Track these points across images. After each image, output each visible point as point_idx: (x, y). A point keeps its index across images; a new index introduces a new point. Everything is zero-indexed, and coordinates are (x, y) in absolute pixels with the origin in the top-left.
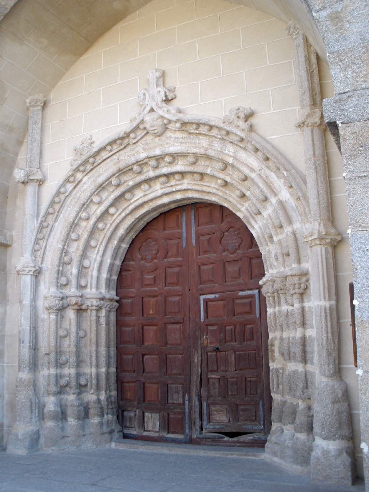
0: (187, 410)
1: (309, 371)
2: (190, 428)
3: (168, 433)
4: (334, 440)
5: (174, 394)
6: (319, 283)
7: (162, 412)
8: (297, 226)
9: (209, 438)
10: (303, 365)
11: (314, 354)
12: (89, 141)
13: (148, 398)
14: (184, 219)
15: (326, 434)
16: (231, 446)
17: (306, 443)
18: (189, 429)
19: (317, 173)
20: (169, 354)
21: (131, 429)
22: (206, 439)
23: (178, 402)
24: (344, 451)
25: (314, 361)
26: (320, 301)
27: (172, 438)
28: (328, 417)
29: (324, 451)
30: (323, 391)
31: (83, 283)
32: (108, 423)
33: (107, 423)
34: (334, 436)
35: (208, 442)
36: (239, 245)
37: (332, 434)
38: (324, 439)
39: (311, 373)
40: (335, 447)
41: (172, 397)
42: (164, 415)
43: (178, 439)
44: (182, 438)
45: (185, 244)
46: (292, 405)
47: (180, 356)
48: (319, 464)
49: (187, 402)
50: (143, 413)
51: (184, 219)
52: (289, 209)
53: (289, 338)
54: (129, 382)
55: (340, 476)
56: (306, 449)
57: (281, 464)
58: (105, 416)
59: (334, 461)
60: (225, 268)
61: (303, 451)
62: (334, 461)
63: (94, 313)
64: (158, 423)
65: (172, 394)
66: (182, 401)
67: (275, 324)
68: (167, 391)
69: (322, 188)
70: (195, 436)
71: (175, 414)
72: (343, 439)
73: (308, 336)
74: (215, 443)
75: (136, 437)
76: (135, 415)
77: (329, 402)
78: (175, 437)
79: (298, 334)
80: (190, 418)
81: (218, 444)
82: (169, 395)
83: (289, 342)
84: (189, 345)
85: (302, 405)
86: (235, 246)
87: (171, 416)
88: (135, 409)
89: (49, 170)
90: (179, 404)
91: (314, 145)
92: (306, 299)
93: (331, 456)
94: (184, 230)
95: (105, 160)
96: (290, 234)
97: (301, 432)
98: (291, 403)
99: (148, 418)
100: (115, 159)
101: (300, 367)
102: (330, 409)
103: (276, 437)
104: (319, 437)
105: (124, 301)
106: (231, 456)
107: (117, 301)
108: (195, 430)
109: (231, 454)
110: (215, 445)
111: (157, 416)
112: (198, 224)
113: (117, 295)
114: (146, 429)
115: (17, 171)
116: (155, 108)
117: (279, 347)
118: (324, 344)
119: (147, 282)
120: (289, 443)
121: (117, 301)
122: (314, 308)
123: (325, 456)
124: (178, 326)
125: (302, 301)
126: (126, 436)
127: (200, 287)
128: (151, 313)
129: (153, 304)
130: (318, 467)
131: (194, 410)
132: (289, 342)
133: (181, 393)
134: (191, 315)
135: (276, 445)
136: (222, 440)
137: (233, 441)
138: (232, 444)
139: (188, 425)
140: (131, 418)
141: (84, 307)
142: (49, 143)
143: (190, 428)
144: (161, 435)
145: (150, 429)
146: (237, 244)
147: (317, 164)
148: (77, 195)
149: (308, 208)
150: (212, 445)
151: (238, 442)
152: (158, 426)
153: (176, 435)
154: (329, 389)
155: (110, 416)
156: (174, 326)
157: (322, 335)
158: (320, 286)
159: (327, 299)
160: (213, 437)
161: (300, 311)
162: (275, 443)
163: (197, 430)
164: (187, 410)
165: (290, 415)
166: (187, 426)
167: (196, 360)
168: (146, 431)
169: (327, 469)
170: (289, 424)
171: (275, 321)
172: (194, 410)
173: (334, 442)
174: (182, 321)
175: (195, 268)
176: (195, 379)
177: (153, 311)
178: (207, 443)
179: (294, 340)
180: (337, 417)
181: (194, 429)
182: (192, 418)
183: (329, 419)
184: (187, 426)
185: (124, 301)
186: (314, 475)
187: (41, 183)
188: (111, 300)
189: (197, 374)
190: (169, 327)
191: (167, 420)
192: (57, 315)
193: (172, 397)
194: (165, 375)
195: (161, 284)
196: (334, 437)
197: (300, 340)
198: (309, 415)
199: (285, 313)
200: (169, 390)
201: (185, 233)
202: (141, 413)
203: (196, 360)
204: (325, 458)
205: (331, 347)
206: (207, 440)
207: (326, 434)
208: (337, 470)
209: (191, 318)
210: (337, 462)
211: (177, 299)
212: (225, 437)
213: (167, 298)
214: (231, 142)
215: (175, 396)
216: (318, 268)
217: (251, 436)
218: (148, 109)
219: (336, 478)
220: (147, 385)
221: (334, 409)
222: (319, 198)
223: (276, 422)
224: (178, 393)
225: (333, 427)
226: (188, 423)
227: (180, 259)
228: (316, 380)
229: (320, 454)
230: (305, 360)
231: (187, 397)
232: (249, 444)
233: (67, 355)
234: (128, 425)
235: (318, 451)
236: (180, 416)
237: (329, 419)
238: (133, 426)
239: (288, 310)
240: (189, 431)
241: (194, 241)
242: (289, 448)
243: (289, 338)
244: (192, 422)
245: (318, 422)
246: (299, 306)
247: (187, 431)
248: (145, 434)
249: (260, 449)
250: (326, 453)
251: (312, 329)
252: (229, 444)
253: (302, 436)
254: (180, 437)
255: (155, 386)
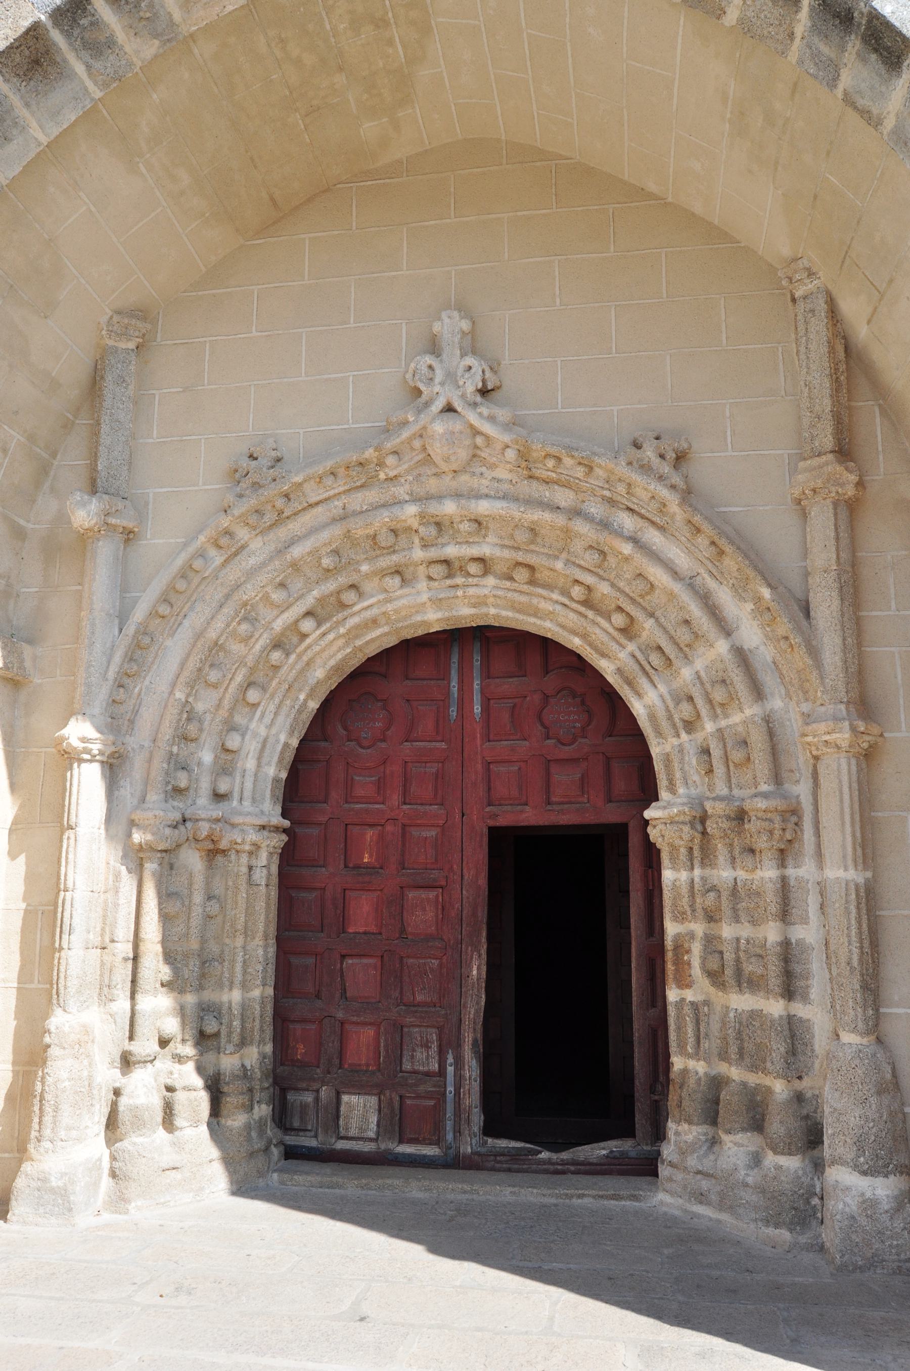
0: (450, 1088)
1: (794, 1015)
2: (458, 1132)
3: (401, 1142)
4: (886, 1176)
5: (419, 1050)
6: (843, 831)
7: (388, 1093)
8: (776, 703)
9: (503, 1155)
10: (786, 1002)
11: (810, 982)
12: (274, 454)
13: (351, 1059)
14: (455, 659)
15: (867, 1163)
16: (557, 1172)
17: (800, 1178)
18: (454, 1132)
19: (842, 600)
20: (408, 957)
21: (301, 1134)
22: (495, 1156)
23: (426, 1069)
24: (906, 1200)
25: (812, 997)
26: (846, 869)
27: (410, 1155)
28: (872, 1124)
29: (864, 1202)
30: (853, 1066)
31: (223, 788)
32: (261, 1123)
33: (258, 1124)
34: (884, 1166)
35: (500, 1162)
36: (583, 729)
37: (880, 1163)
38: (864, 1173)
39: (801, 1020)
40: (889, 1192)
41: (413, 1055)
42: (391, 1099)
43: (425, 1156)
44: (437, 1153)
45: (455, 714)
46: (745, 1088)
47: (436, 962)
48: (856, 1232)
49: (450, 1070)
50: (338, 1094)
51: (455, 659)
52: (757, 664)
53: (738, 940)
54: (303, 1021)
55: (903, 1256)
56: (801, 1191)
57: (719, 1221)
58: (256, 1107)
59: (889, 1224)
60: (548, 774)
61: (796, 1196)
62: (889, 1224)
63: (244, 859)
64: (374, 1119)
65: (414, 1050)
66: (437, 1066)
67: (690, 906)
68: (401, 1044)
69: (851, 632)
70: (469, 1150)
71: (418, 1097)
72: (901, 1173)
73: (793, 941)
74: (516, 1166)
75: (318, 1153)
76: (317, 1099)
77: (872, 1091)
78: (418, 1153)
79: (772, 933)
80: (457, 1105)
81: (525, 1167)
82: (405, 1052)
83: (738, 949)
84: (460, 936)
85: (780, 1088)
86: (575, 727)
87: (408, 1102)
88: (315, 1086)
89: (150, 507)
90: (428, 1074)
91: (837, 539)
92: (790, 861)
93: (882, 1211)
94: (454, 683)
95: (311, 506)
96: (760, 721)
97: (790, 1154)
98: (744, 1084)
99: (351, 1107)
100: (335, 507)
101: (775, 1008)
102: (874, 1106)
103: (697, 1156)
104: (850, 1170)
105: (299, 830)
106: (580, 1201)
107: (285, 831)
108: (469, 1135)
109: (580, 1196)
110: (518, 1171)
111: (373, 1101)
112: (487, 674)
113: (284, 815)
114: (343, 1132)
115: (79, 499)
116: (458, 405)
117: (701, 957)
118: (855, 962)
119: (359, 792)
120: (747, 1175)
121: (285, 831)
122: (810, 882)
123: (869, 1212)
124: (432, 894)
125: (782, 864)
126: (292, 1153)
127: (488, 809)
128: (366, 860)
129: (371, 841)
130: (854, 1237)
131: (467, 1087)
132: (738, 949)
133: (435, 1047)
134: (465, 871)
135: (699, 1177)
136: (534, 1157)
137: (562, 1160)
138: (559, 1167)
139: (452, 1122)
140: (304, 1107)
141: (223, 845)
142: (151, 441)
143: (458, 1132)
144: (383, 1146)
145: (353, 1132)
146: (578, 725)
147: (843, 581)
148: (231, 578)
149: (818, 672)
150: (509, 1170)
151: (574, 1163)
152: (373, 1126)
153: (419, 1147)
154: (866, 1061)
155: (264, 1106)
156: (423, 894)
157: (850, 944)
158: (844, 838)
159: (860, 868)
160: (514, 1152)
161: (779, 886)
162: (699, 1172)
163: (475, 1136)
164: (450, 1088)
165: (745, 1112)
166: (449, 1125)
167: (475, 972)
168: (342, 1138)
169: (874, 1240)
170: (742, 1130)
171: (691, 898)
172: (467, 1087)
173: (886, 1179)
174: (443, 883)
175: (479, 766)
176: (472, 1016)
177: (371, 856)
178: (498, 1165)
179: (750, 946)
180: (889, 1125)
181: (467, 1132)
182: (463, 1107)
183: (874, 1130)
184: (449, 1125)
185: (299, 830)
186: (843, 1255)
187: (131, 536)
188: (277, 829)
189: (478, 1003)
190: (411, 894)
191: (397, 1112)
192: (160, 864)
193: (412, 1057)
194: (398, 1005)
195: (395, 797)
196: (885, 1171)
197: (779, 948)
198: (801, 1113)
199: (730, 885)
200: (406, 1039)
201: (456, 688)
202: (333, 1094)
203: (475, 972)
204: (867, 1216)
205: (867, 970)
206: (498, 1158)
207: (867, 1163)
208: (895, 1243)
209: (466, 878)
210: (895, 1225)
211: (432, 833)
212: (540, 1152)
213: (407, 828)
214: (629, 509)
215: (420, 1054)
216: (841, 801)
217: (604, 1149)
218: (439, 404)
219: (894, 1262)
220: (348, 1027)
221: (884, 1106)
222: (845, 654)
223: (698, 1124)
224: (428, 1048)
225: (883, 1146)
226: (452, 1117)
227: (443, 745)
228: (817, 1037)
229: (854, 1208)
230: (789, 993)
231: (450, 1059)
232: (599, 1168)
233: (175, 960)
234: (296, 1124)
235: (848, 1200)
236: (432, 1103)
237: (874, 1130)
238: (310, 1128)
239: (735, 879)
240: (455, 1137)
241: (477, 709)
242: (746, 1185)
243: (738, 940)
244: (462, 1116)
245: (844, 1135)
246: (777, 875)
247: (450, 1137)
248: (341, 1145)
249: (642, 1181)
250: (869, 1205)
251: (805, 926)
252: (551, 1167)
253: (792, 1163)
254: (430, 1151)
255: (370, 1032)
